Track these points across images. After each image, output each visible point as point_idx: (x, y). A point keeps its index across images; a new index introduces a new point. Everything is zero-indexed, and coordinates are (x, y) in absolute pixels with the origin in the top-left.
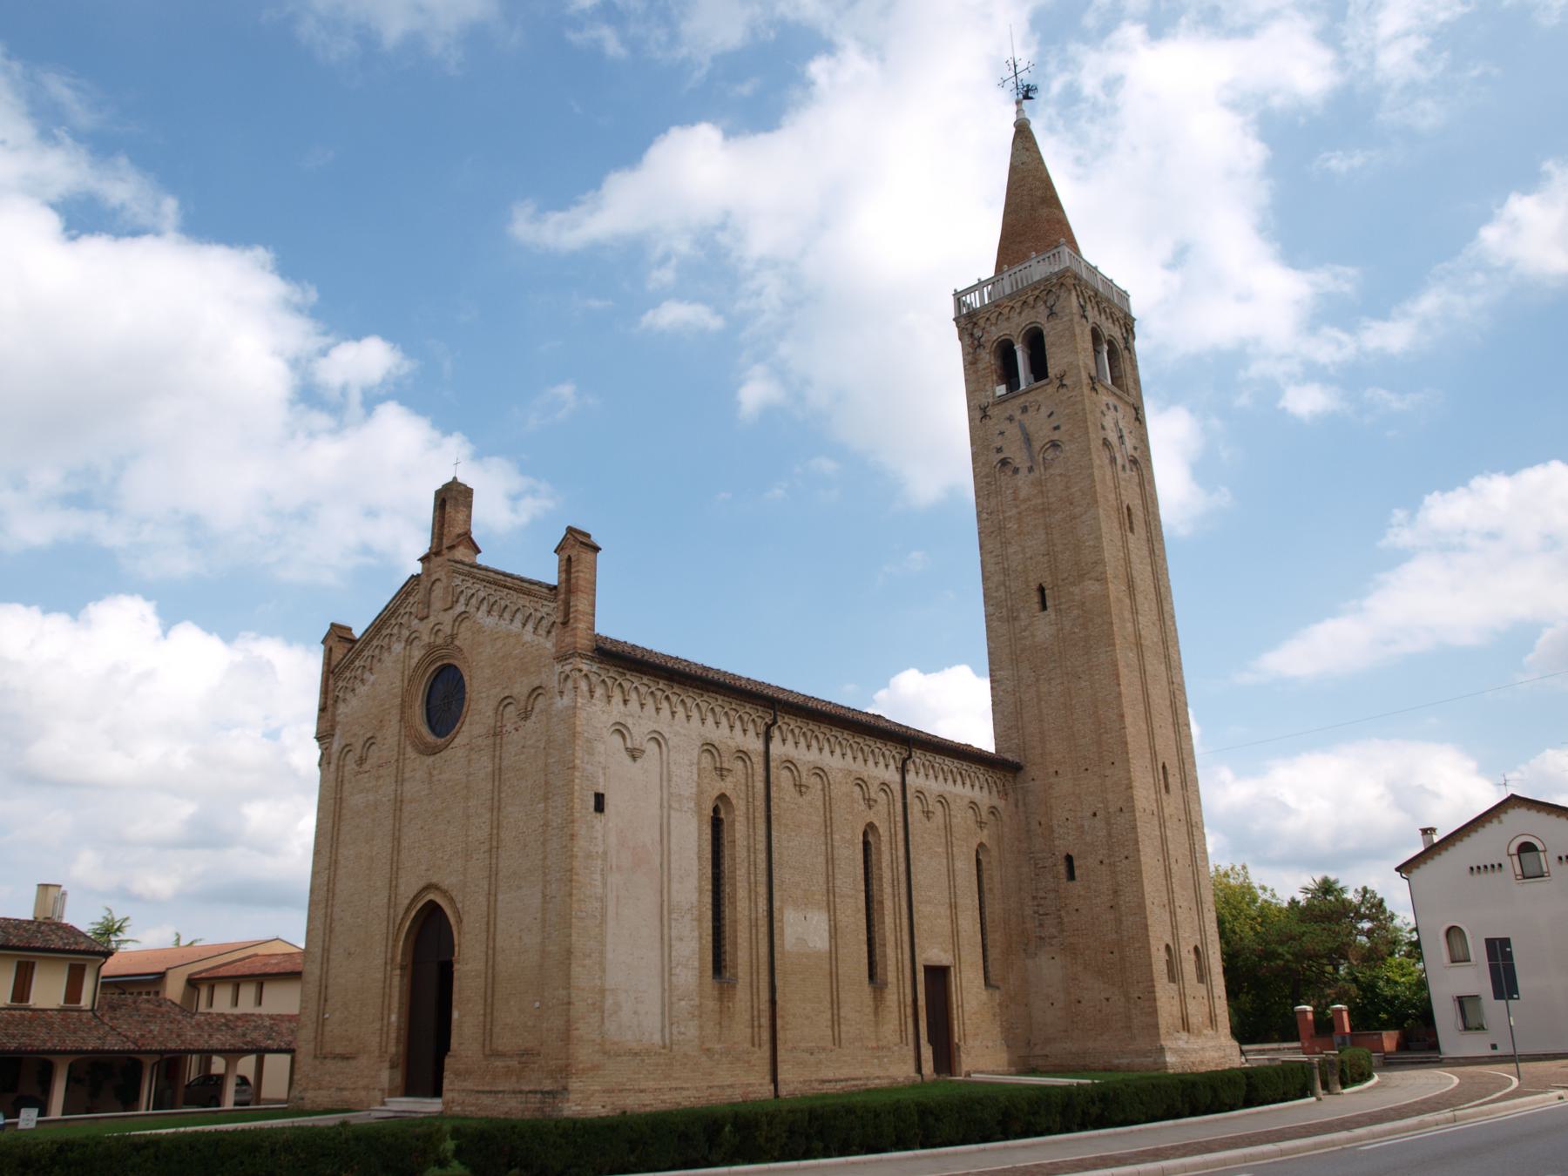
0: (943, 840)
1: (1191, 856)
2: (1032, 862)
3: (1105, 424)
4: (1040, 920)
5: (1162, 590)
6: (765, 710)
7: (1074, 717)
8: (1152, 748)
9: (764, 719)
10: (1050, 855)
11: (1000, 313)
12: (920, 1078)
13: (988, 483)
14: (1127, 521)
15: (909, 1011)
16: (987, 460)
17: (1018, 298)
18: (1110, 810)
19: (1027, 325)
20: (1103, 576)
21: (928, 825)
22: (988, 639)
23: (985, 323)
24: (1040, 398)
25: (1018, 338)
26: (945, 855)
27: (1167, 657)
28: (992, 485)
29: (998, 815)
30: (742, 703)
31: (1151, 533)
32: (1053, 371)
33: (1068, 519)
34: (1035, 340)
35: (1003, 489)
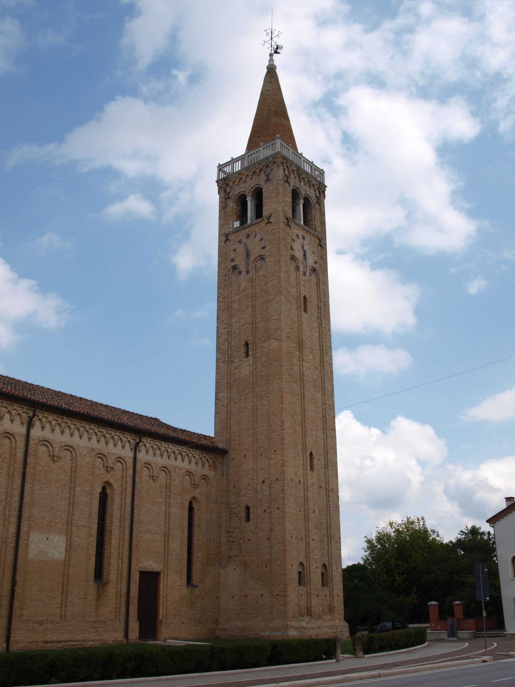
0: (164, 494)
1: (327, 509)
2: (228, 510)
3: (294, 247)
4: (230, 545)
5: (325, 348)
6: (29, 408)
7: (258, 423)
8: (304, 443)
9: (28, 414)
10: (238, 506)
11: (241, 178)
12: (126, 641)
13: (225, 280)
14: (303, 306)
15: (124, 599)
16: (225, 266)
17: (251, 170)
18: (272, 479)
19: (254, 186)
20: (280, 337)
21: (153, 484)
22: (216, 374)
23: (233, 184)
24: (257, 230)
25: (249, 194)
26: (164, 504)
27: (323, 389)
28: (227, 281)
29: (208, 480)
30: (12, 403)
31: (321, 314)
32: (265, 214)
33: (265, 302)
34: (258, 194)
35: (233, 283)
